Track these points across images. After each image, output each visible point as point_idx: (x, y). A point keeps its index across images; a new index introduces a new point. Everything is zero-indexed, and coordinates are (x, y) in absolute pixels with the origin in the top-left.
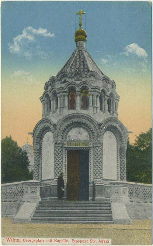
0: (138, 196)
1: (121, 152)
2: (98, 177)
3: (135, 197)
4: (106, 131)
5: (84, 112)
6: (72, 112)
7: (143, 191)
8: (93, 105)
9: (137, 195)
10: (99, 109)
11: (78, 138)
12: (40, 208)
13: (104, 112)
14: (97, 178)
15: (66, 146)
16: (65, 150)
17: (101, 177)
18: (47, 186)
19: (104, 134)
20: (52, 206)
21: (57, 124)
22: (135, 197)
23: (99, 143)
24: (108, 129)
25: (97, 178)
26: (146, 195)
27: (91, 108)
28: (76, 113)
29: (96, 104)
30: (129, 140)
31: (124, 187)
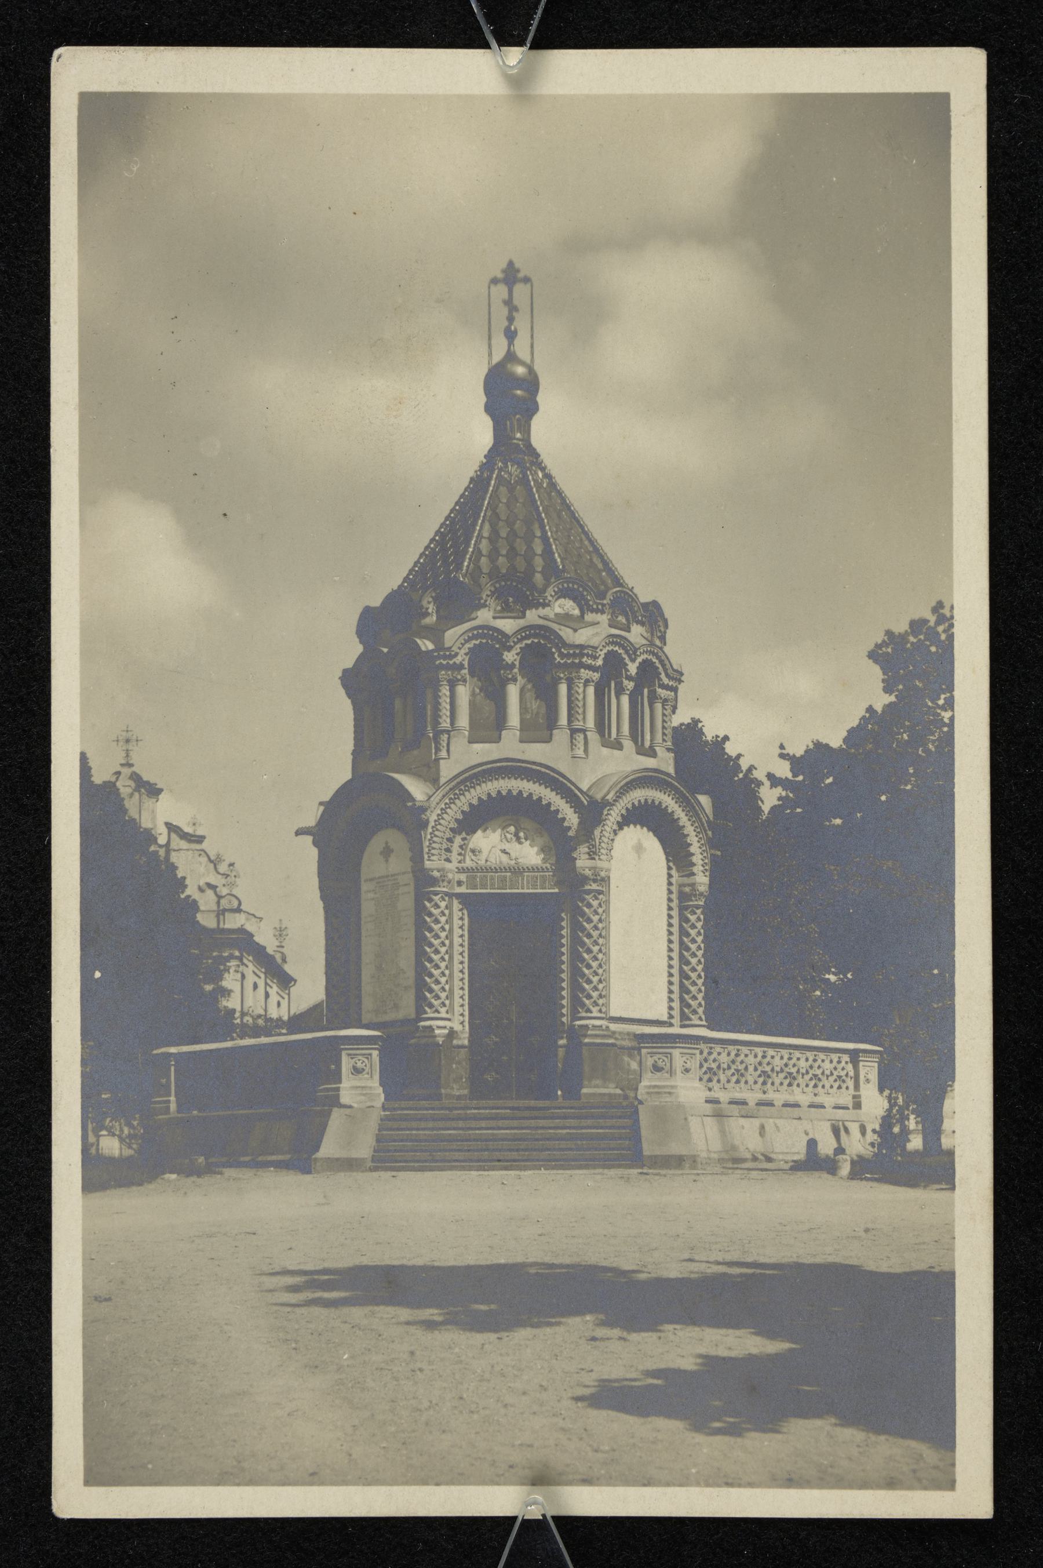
0: (839, 1087)
1: (686, 908)
2: (591, 1012)
3: (831, 1091)
4: (621, 828)
5: (535, 752)
6: (484, 752)
7: (835, 1069)
8: (570, 721)
9: (836, 1085)
10: (593, 737)
11: (513, 855)
12: (390, 1124)
13: (618, 746)
14: (589, 1015)
15: (463, 890)
16: (461, 907)
17: (604, 1010)
18: (606, 1041)
19: (613, 840)
20: (434, 1119)
21: (426, 804)
22: (831, 1091)
23: (595, 881)
24: (630, 818)
25: (589, 1015)
26: (844, 1081)
27: (561, 736)
28: (656, 770)
29: (580, 717)
30: (389, 844)
31: (655, 1050)
